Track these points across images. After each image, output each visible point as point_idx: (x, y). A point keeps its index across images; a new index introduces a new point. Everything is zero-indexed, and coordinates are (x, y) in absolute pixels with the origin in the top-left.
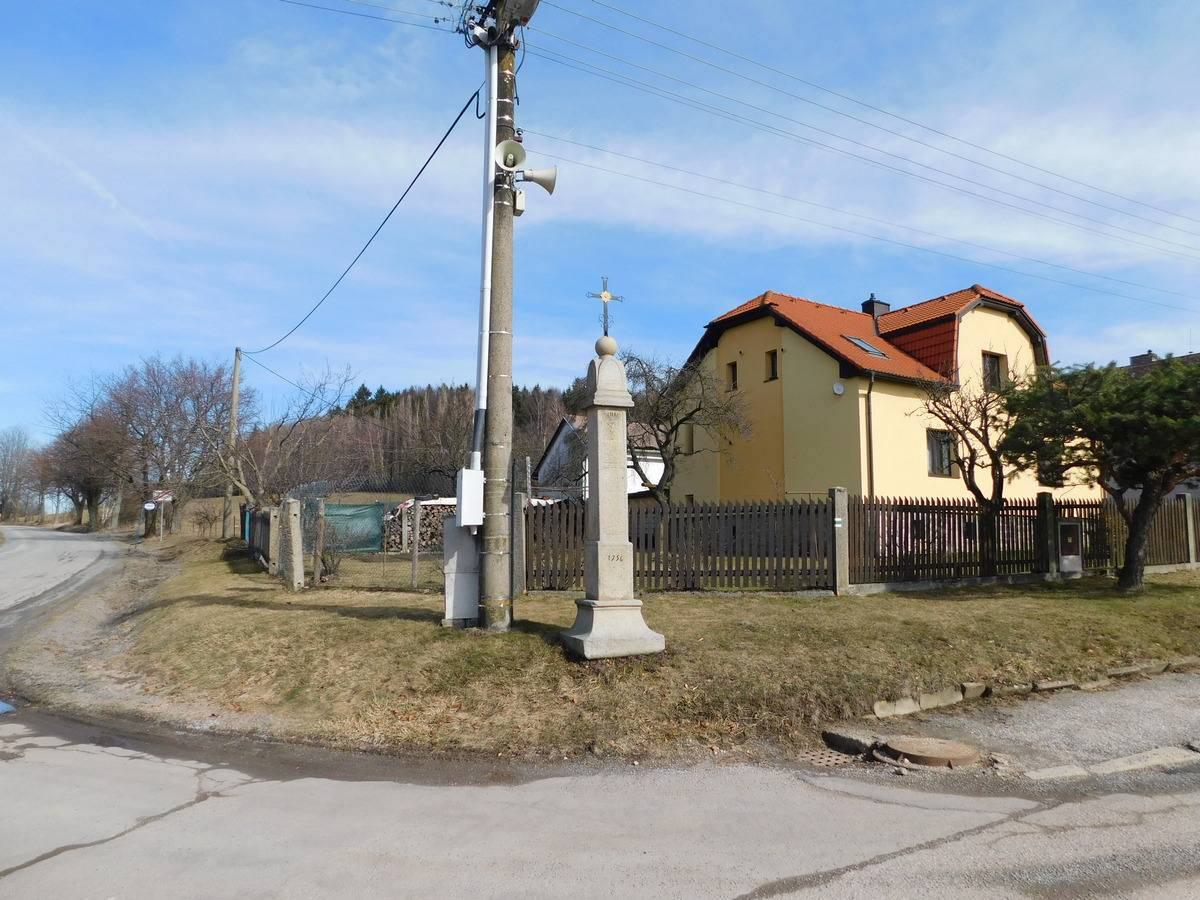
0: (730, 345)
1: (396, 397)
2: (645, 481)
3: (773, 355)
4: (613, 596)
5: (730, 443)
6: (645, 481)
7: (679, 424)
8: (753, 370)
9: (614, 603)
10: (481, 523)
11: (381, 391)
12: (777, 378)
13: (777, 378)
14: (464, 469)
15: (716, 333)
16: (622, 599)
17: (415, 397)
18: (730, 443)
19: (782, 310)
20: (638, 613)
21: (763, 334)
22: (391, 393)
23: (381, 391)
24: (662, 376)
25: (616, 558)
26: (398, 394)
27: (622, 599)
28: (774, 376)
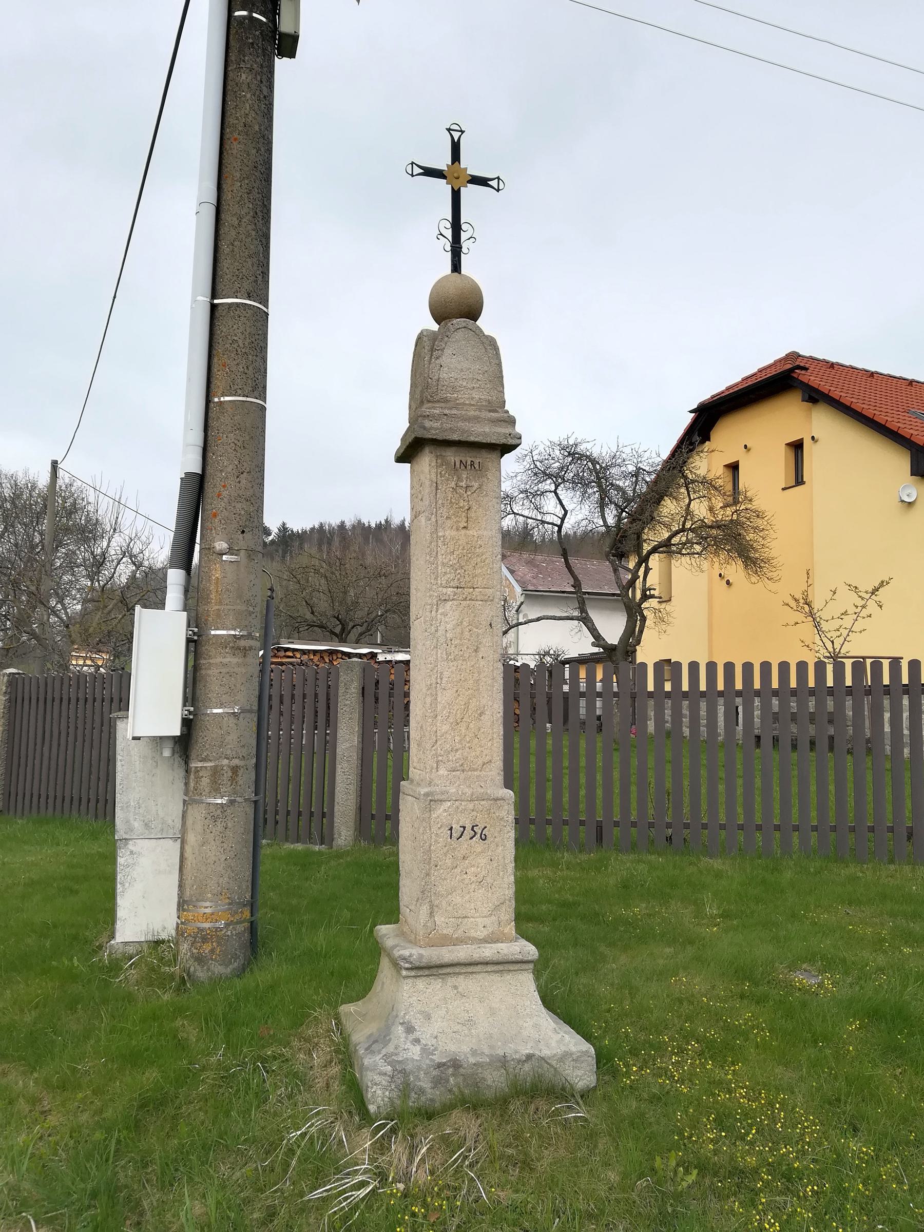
0: (727, 440)
1: (302, 537)
2: (598, 638)
3: (797, 447)
4: (459, 933)
5: (728, 583)
6: (598, 638)
7: (650, 553)
8: (763, 478)
9: (462, 953)
10: (177, 732)
11: (284, 528)
12: (803, 483)
13: (803, 483)
14: (138, 608)
15: (708, 418)
16: (485, 941)
17: (321, 535)
18: (728, 583)
19: (811, 378)
20: (525, 986)
21: (784, 419)
22: (295, 530)
23: (284, 528)
24: (625, 484)
25: (468, 833)
26: (304, 532)
27: (485, 941)
28: (799, 481)
